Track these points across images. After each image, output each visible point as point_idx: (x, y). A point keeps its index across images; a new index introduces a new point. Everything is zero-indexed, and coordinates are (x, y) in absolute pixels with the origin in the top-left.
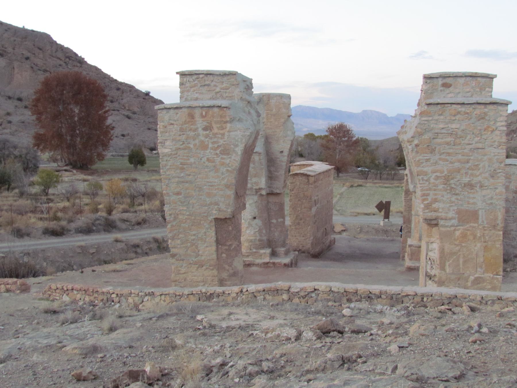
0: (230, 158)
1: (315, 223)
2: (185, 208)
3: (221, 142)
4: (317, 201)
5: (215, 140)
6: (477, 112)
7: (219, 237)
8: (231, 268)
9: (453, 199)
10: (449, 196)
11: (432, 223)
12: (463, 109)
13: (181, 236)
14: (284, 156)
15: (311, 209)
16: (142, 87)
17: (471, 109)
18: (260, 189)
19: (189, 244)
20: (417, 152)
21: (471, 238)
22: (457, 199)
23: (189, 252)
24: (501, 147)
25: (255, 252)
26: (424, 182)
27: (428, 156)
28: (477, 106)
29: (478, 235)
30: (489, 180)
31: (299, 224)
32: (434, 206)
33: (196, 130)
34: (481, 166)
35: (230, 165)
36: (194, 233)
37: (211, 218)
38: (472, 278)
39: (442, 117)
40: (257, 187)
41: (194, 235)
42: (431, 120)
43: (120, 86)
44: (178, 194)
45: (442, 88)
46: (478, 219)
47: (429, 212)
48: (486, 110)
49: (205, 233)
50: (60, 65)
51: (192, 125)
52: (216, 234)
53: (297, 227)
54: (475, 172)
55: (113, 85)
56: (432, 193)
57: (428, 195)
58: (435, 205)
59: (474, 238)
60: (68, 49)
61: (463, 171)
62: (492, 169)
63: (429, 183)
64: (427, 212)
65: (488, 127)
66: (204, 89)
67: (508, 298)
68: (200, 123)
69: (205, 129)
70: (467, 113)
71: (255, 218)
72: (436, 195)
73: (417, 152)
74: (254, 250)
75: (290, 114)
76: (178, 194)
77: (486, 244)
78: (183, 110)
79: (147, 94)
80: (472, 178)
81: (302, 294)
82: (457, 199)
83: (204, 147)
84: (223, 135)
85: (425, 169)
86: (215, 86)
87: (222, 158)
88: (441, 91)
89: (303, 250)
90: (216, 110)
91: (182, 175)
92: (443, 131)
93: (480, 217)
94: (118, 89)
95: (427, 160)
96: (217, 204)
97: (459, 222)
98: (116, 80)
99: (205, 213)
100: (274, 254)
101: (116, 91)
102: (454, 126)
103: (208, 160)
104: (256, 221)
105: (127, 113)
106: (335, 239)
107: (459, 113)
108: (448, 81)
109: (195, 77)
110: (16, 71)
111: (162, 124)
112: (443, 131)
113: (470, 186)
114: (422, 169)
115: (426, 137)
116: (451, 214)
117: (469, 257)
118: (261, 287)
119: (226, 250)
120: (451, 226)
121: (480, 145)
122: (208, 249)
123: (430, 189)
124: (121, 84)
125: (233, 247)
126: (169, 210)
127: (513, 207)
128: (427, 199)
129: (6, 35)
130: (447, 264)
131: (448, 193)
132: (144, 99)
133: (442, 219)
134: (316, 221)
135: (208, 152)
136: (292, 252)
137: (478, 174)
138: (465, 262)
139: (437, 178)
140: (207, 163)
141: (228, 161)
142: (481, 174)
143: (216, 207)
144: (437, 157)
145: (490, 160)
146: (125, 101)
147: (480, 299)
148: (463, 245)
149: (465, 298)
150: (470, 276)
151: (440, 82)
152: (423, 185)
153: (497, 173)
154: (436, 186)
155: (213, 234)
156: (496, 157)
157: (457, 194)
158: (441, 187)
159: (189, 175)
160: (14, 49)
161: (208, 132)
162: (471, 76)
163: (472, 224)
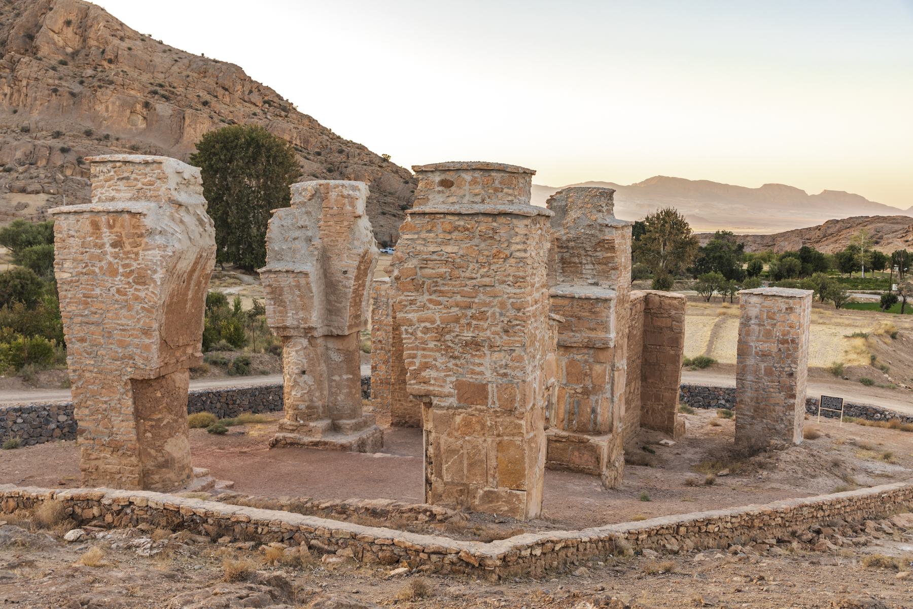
0: (147, 289)
2: (92, 362)
3: (135, 265)
5: (127, 262)
6: (483, 227)
7: (140, 408)
8: (159, 454)
9: (450, 365)
10: (444, 359)
12: (462, 223)
13: (89, 403)
14: (348, 278)
17: (473, 222)
19: (100, 416)
21: (478, 427)
22: (456, 365)
23: (101, 428)
24: (518, 284)
25: (303, 425)
27: (413, 295)
28: (481, 218)
29: (488, 423)
30: (501, 338)
32: (423, 374)
33: (102, 246)
34: (489, 314)
35: (146, 300)
36: (104, 399)
37: (125, 378)
38: (481, 492)
39: (432, 235)
40: (306, 326)
41: (106, 402)
42: (417, 239)
43: (344, 147)
44: (82, 340)
45: (440, 188)
46: (487, 398)
48: (495, 224)
49: (119, 400)
50: (255, 114)
51: (97, 238)
52: (134, 403)
54: (482, 323)
55: (335, 146)
56: (420, 353)
59: (482, 429)
60: (268, 88)
61: (463, 321)
62: (506, 320)
63: (416, 338)
64: (414, 384)
65: (499, 252)
66: (122, 185)
67: (364, 538)
68: (107, 237)
69: (114, 245)
70: (468, 229)
71: (304, 372)
72: (424, 356)
73: (398, 289)
74: (302, 422)
76: (82, 340)
77: (500, 438)
78: (86, 216)
80: (477, 332)
81: (115, 508)
82: (456, 365)
83: (113, 272)
84: (137, 254)
85: (410, 316)
86: (136, 179)
87: (136, 290)
88: (439, 192)
89: (410, 423)
90: (127, 216)
91: (86, 312)
92: (435, 257)
93: (490, 396)
94: (341, 152)
95: (412, 302)
96: (132, 358)
97: (460, 402)
98: (339, 137)
99: (117, 370)
101: (337, 155)
102: (449, 249)
103: (118, 291)
104: (305, 377)
107: (456, 228)
108: (449, 176)
109: (111, 165)
110: (187, 121)
111: (59, 235)
112: (435, 257)
113: (475, 345)
114: (405, 315)
115: (411, 264)
116: (448, 389)
117: (476, 458)
119: (152, 426)
120: (448, 408)
121: (487, 280)
122: (124, 424)
123: (417, 348)
125: (165, 422)
126: (73, 364)
127: (778, 365)
129: (175, 68)
130: (444, 467)
131: (442, 355)
132: (380, 166)
133: (435, 396)
135: (117, 279)
137: (486, 325)
138: (471, 465)
139: (426, 330)
140: (117, 295)
141: (142, 294)
142: (490, 326)
143: (131, 362)
144: (426, 297)
145: (502, 305)
146: (349, 170)
147: (328, 536)
148: (467, 438)
149: (311, 533)
150: (477, 488)
151: (437, 178)
153: (513, 326)
154: (424, 342)
155: (130, 402)
156: (511, 300)
157: (455, 358)
158: (432, 345)
159: (95, 313)
161: (117, 250)
162: (481, 170)
163: (478, 407)
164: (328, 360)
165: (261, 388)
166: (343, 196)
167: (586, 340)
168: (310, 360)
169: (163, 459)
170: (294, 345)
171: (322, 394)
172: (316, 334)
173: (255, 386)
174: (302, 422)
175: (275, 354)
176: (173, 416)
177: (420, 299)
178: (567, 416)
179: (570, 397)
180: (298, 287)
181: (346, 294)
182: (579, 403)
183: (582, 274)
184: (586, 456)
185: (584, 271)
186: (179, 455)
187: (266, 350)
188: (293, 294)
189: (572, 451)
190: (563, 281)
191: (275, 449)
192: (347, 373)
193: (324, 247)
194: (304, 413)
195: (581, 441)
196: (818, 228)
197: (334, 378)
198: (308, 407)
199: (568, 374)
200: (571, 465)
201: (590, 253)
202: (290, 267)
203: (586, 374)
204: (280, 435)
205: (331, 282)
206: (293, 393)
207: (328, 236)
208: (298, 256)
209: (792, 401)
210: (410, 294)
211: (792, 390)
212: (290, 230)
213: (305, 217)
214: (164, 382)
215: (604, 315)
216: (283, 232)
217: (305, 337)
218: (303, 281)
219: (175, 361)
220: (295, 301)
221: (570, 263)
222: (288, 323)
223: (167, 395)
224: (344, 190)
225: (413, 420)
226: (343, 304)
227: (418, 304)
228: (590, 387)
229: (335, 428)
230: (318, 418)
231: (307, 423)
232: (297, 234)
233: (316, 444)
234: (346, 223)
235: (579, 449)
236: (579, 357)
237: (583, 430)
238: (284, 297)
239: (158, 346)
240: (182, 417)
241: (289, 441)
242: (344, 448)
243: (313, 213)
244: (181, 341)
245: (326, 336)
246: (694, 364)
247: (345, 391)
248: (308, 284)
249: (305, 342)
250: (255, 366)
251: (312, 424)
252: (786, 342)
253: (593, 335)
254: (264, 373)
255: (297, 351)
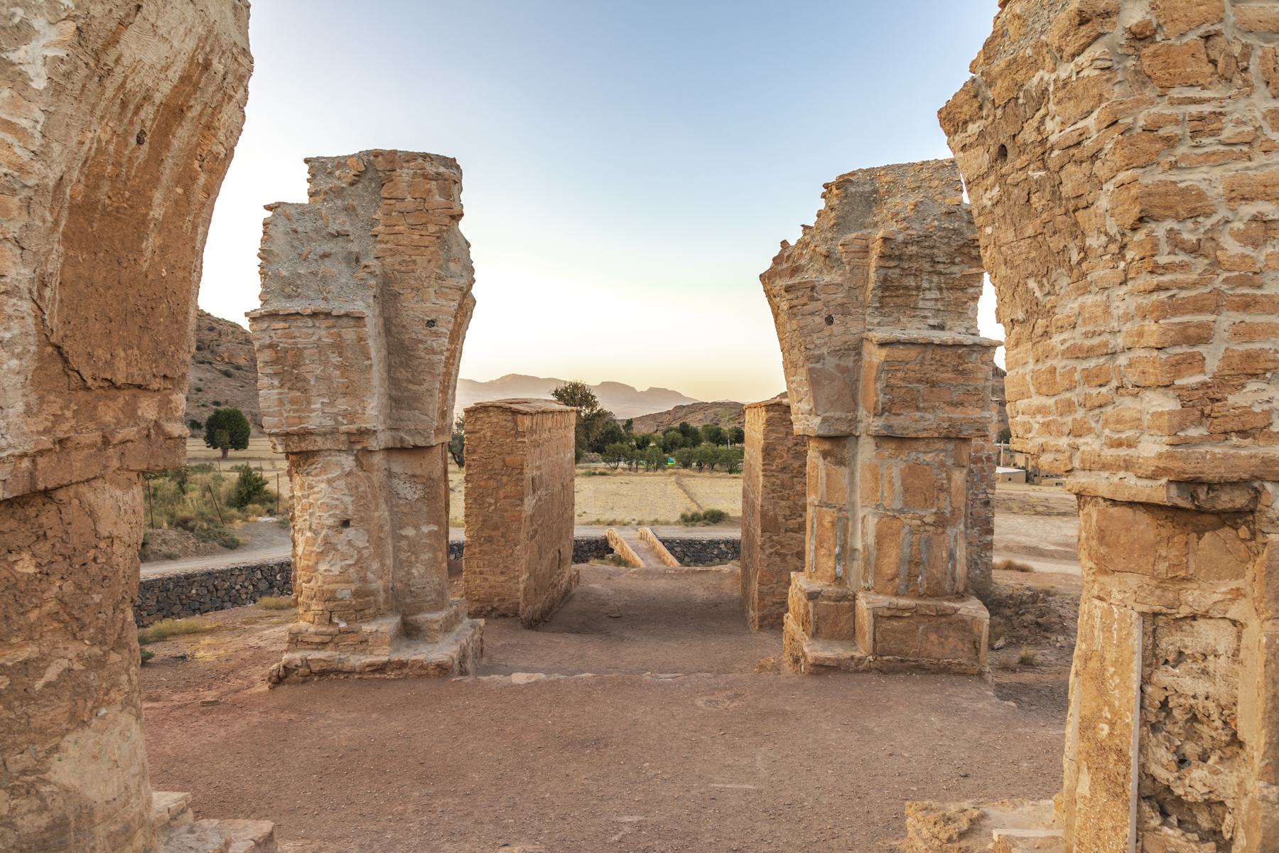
1: (533, 537)
4: (537, 481)
8: (24, 804)
11: (1232, 501)
15: (522, 500)
18: (364, 433)
20: (1143, 79)
26: (1181, 257)
31: (490, 540)
32: (1234, 399)
40: (353, 428)
43: (215, 325)
47: (1210, 438)
53: (486, 547)
56: (1226, 320)
57: (1202, 336)
58: (1248, 397)
64: (1202, 441)
71: (346, 523)
74: (343, 625)
75: (455, 211)
85: (1192, 179)
89: (502, 609)
94: (211, 329)
95: (1202, 126)
100: (409, 632)
104: (350, 533)
105: (223, 368)
106: (578, 572)
114: (1174, 176)
118: (853, 235)
123: (1216, 304)
124: (218, 321)
125: (51, 674)
128: (1195, 362)
134: (536, 531)
136: (467, 621)
146: (222, 348)
152: (1180, 277)
164: (392, 496)
165: (178, 577)
166: (425, 176)
167: (946, 425)
168: (359, 497)
169: (44, 820)
170: (324, 470)
171: (383, 565)
172: (373, 444)
173: (167, 575)
174: (343, 625)
175: (186, 529)
176: (85, 648)
177: (1238, 109)
178: (904, 570)
179: (912, 532)
180: (338, 347)
181: (431, 365)
182: (928, 542)
183: (915, 308)
184: (953, 641)
185: (921, 304)
186: (111, 790)
187: (170, 524)
188: (326, 363)
189: (925, 633)
190: (879, 324)
191: (284, 689)
192: (428, 523)
193: (385, 274)
194: (348, 607)
195: (942, 614)
196: (668, 413)
197: (404, 532)
198: (356, 594)
199: (906, 490)
200: (924, 661)
201: (940, 267)
202: (321, 306)
203: (941, 489)
204: (296, 656)
205: (402, 343)
206: (322, 567)
207: (393, 253)
208: (333, 288)
209: (989, 538)
210: (1195, 93)
211: (989, 523)
212: (310, 240)
213: (342, 217)
214: (49, 518)
215: (980, 375)
216: (296, 243)
217: (348, 451)
218: (349, 335)
219: (96, 437)
220: (329, 379)
221: (897, 288)
222: (313, 423)
223: (62, 566)
224: (427, 165)
225: (506, 604)
226: (426, 386)
227: (1228, 132)
228: (947, 511)
229: (409, 632)
230: (378, 615)
231: (355, 626)
232: (327, 247)
233: (381, 668)
234: (432, 229)
235: (937, 630)
236: (928, 458)
237: (935, 592)
238: (303, 369)
239: (30, 363)
240: (120, 645)
241: (315, 668)
242: (442, 670)
243: (360, 211)
244: (121, 365)
245: (389, 450)
246: (705, 518)
247: (426, 556)
248: (361, 339)
249: (348, 462)
250: (155, 547)
251: (367, 628)
252: (980, 460)
253: (957, 414)
254: (170, 557)
255: (330, 482)
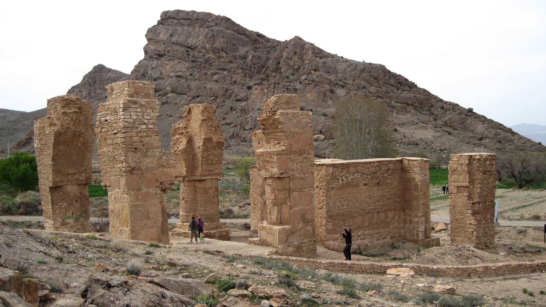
16: (465, 104)
60: (400, 76)
79: (470, 110)
124: (446, 103)
160: (354, 81)
